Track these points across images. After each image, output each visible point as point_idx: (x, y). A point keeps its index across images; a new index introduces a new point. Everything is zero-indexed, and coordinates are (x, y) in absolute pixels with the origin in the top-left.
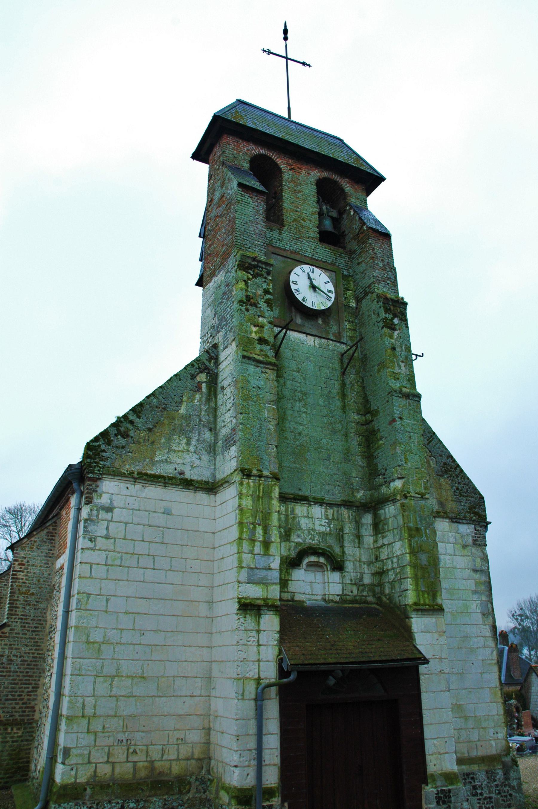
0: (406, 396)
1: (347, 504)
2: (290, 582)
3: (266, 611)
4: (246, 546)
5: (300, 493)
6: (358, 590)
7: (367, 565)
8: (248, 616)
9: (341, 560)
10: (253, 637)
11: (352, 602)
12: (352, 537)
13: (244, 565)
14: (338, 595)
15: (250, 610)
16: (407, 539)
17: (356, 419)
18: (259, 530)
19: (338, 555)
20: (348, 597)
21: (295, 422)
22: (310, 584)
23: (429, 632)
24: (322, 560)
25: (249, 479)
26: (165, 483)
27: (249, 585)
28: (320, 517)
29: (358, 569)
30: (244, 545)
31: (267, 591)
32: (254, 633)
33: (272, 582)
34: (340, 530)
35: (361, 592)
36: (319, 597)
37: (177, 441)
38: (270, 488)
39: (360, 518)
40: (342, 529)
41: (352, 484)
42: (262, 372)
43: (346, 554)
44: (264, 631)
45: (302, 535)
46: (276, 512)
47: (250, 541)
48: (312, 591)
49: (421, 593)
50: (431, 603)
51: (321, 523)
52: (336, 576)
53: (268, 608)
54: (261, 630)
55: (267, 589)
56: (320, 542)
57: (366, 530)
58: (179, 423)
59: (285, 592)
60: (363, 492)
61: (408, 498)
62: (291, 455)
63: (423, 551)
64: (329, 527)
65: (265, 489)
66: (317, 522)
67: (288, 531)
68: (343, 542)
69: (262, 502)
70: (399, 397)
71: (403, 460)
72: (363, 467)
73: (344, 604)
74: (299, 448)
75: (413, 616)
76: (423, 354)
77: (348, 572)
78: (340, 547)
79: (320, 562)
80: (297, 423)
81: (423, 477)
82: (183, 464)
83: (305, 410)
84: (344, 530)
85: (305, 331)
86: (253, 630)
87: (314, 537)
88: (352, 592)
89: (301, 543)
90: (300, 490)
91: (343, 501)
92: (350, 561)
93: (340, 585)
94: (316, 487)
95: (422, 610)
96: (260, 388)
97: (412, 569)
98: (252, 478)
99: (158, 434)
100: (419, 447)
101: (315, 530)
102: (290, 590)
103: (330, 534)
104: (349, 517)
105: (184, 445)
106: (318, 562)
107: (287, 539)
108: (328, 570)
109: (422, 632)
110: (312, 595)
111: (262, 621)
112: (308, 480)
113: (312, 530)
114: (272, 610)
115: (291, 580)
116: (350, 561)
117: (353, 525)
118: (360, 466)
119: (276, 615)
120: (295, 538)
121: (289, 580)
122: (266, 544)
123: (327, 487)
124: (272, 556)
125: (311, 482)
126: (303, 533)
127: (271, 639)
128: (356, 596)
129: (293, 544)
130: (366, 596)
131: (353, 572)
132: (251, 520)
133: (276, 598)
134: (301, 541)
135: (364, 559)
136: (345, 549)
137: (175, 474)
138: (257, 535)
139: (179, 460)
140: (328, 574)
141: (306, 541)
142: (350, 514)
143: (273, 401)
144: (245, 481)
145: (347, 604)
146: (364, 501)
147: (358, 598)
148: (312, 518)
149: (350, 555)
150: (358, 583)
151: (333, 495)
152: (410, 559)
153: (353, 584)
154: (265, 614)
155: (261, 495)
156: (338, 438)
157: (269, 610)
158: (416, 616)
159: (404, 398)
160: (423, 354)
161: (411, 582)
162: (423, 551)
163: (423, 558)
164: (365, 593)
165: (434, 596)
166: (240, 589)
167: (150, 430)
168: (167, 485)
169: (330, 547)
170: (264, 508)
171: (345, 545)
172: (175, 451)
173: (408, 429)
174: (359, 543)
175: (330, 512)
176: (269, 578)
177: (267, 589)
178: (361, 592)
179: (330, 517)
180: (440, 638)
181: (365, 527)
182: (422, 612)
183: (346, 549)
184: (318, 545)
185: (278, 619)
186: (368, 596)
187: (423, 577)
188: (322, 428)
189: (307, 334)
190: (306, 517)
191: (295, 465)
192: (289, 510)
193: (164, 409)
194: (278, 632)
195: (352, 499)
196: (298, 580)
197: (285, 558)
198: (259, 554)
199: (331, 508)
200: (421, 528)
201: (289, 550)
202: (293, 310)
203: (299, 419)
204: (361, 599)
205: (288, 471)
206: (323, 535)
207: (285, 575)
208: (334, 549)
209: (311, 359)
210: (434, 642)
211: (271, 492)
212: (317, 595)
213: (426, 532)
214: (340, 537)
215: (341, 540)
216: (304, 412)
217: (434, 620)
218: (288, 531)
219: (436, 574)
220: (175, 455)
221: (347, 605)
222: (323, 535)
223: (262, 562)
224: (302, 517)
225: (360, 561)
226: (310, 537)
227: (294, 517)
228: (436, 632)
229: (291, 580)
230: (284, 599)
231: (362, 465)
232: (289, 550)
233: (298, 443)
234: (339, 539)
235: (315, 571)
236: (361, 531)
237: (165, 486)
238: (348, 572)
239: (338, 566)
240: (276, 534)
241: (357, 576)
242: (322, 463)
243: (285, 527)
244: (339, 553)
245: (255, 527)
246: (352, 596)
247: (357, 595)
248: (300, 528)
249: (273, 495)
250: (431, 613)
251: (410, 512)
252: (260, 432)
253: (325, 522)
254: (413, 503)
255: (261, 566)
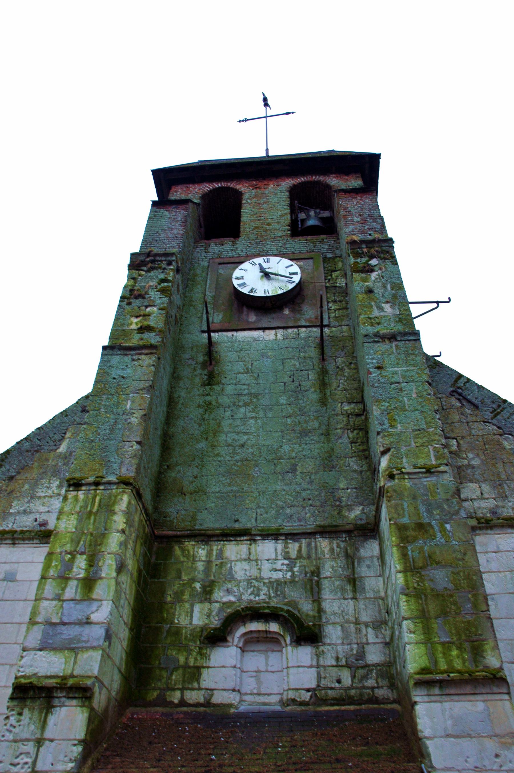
0: (389, 339)
1: (327, 531)
2: (204, 672)
3: (63, 699)
4: (50, 588)
5: (237, 526)
6: (353, 677)
7: (374, 628)
8: (26, 712)
9: (314, 625)
10: (28, 754)
11: (339, 701)
12: (337, 583)
13: (39, 619)
14: (308, 690)
15: (33, 699)
16: (397, 545)
17: (346, 411)
18: (81, 562)
19: (307, 615)
20: (330, 692)
21: (235, 432)
22: (254, 674)
23: (470, 736)
24: (274, 627)
25: (78, 491)
26: (13, 539)
27: (41, 653)
28: (273, 556)
29: (353, 638)
30: (47, 587)
31: (75, 662)
32: (30, 747)
33: (88, 645)
34: (312, 573)
35: (361, 681)
36: (275, 699)
37: (45, 485)
38: (113, 498)
39: (357, 549)
40: (317, 572)
41: (339, 500)
42: (133, 360)
43: (325, 612)
44: (52, 740)
45: (235, 589)
46: (118, 531)
47: (59, 580)
48: (259, 688)
49: (440, 648)
50: (470, 666)
51: (274, 566)
52: (305, 654)
53: (68, 693)
54: (45, 739)
55: (76, 658)
56: (270, 597)
57: (369, 567)
58: (53, 463)
59: (193, 689)
60: (361, 508)
61: (397, 477)
62: (224, 476)
63: (438, 563)
64: (291, 570)
65: (103, 501)
66: (266, 566)
67: (209, 586)
68: (319, 593)
69: (95, 519)
70: (375, 342)
71: (386, 422)
72: (361, 472)
73: (320, 705)
74: (239, 464)
75: (417, 699)
76: (449, 298)
77: (329, 644)
78: (314, 601)
79: (270, 632)
80: (238, 433)
81: (430, 442)
82: (49, 512)
83: (254, 415)
84: (322, 571)
85: (260, 326)
86: (28, 740)
87: (259, 590)
88: (339, 681)
89: (233, 603)
90: (236, 521)
91: (320, 526)
92: (334, 623)
93: (314, 670)
94: (267, 513)
95: (441, 683)
96: (123, 377)
97: (413, 600)
98: (84, 488)
99: (20, 482)
100: (420, 400)
101: (263, 578)
102: (204, 684)
103: (293, 581)
104: (332, 550)
105: (54, 489)
106: (266, 632)
107: (206, 599)
108: (286, 645)
109: (448, 736)
110: (259, 694)
111: (52, 720)
112: (253, 505)
113: (256, 579)
114: (75, 698)
115: (208, 667)
116: (334, 623)
117: (341, 562)
118: (355, 471)
119: (81, 706)
120: (220, 595)
121: (204, 667)
122: (89, 583)
123: (288, 511)
124: (96, 600)
125: (259, 507)
126: (238, 586)
127: (61, 757)
128: (349, 689)
129: (217, 605)
130: (373, 688)
131: (343, 644)
132: (68, 547)
133: (90, 674)
134: (233, 599)
135: (365, 618)
136: (323, 604)
137: (34, 527)
138: (75, 570)
139: (43, 508)
140: (286, 650)
141: (243, 597)
142: (335, 545)
143: (144, 389)
144: (71, 495)
145: (328, 705)
146: (363, 522)
147: (353, 692)
148: (256, 560)
149: (335, 614)
150: (356, 664)
151: (300, 520)
152: (406, 581)
153: (342, 666)
154: (61, 706)
155: (95, 509)
156: (312, 440)
157: (69, 698)
158: (426, 699)
159: (387, 341)
160: (449, 298)
161: (412, 626)
162: (438, 563)
163: (440, 578)
164: (370, 683)
165: (477, 652)
166: (24, 660)
167: (11, 478)
168: (17, 542)
169: (293, 603)
170: (97, 529)
171: (324, 597)
172: (39, 497)
173: (396, 379)
174: (354, 591)
175: (293, 547)
176: (84, 639)
177: (76, 658)
178: (361, 681)
179: (293, 554)
180: (503, 753)
181: (368, 562)
182: (441, 687)
183: (326, 605)
184: (268, 603)
185: (86, 715)
186: (378, 687)
187: (444, 613)
188: (282, 431)
189: (264, 329)
190: (245, 560)
191: (230, 489)
192: (215, 553)
193: (37, 451)
194: (81, 742)
195: (339, 522)
196: (223, 667)
197: (198, 629)
198: (72, 600)
199: (295, 540)
200: (429, 524)
201: (209, 616)
202: (245, 309)
203: (242, 427)
204: (361, 695)
205: (218, 498)
206: (278, 584)
207: (196, 659)
208: (300, 606)
209: (269, 354)
210: (486, 762)
211: (114, 503)
212: (269, 695)
213: (443, 530)
214: (313, 584)
215: (316, 589)
216: (252, 418)
217: (480, 706)
218: (209, 586)
219: (475, 606)
220: (38, 503)
221: (326, 708)
222: (277, 585)
223: (75, 612)
224: (237, 561)
225: (357, 622)
226: (250, 591)
227: (222, 563)
228: (490, 737)
229: (208, 667)
230: (191, 702)
231: (359, 469)
232: (209, 616)
233: (238, 458)
234: (312, 589)
235: (266, 651)
236: (357, 569)
237: (14, 544)
238: (329, 644)
239: (308, 634)
240: (110, 565)
241: (352, 650)
242: (280, 477)
243: (203, 580)
244: (311, 613)
245: (73, 558)
246: (340, 688)
247: (352, 687)
248: (231, 577)
249: (117, 508)
250: (468, 689)
251: (401, 499)
252: (112, 430)
253: (283, 564)
254: (407, 484)
255: (73, 619)
